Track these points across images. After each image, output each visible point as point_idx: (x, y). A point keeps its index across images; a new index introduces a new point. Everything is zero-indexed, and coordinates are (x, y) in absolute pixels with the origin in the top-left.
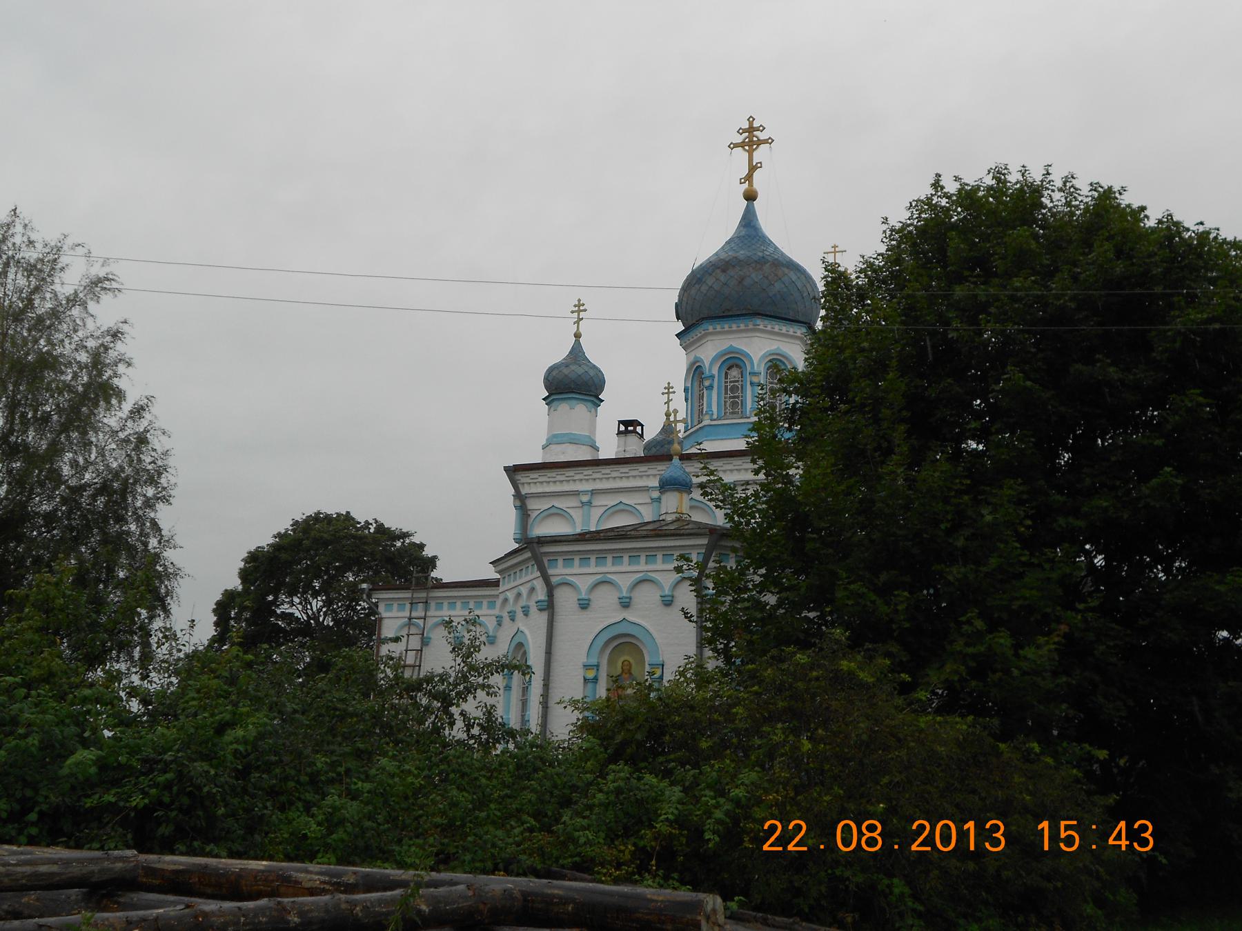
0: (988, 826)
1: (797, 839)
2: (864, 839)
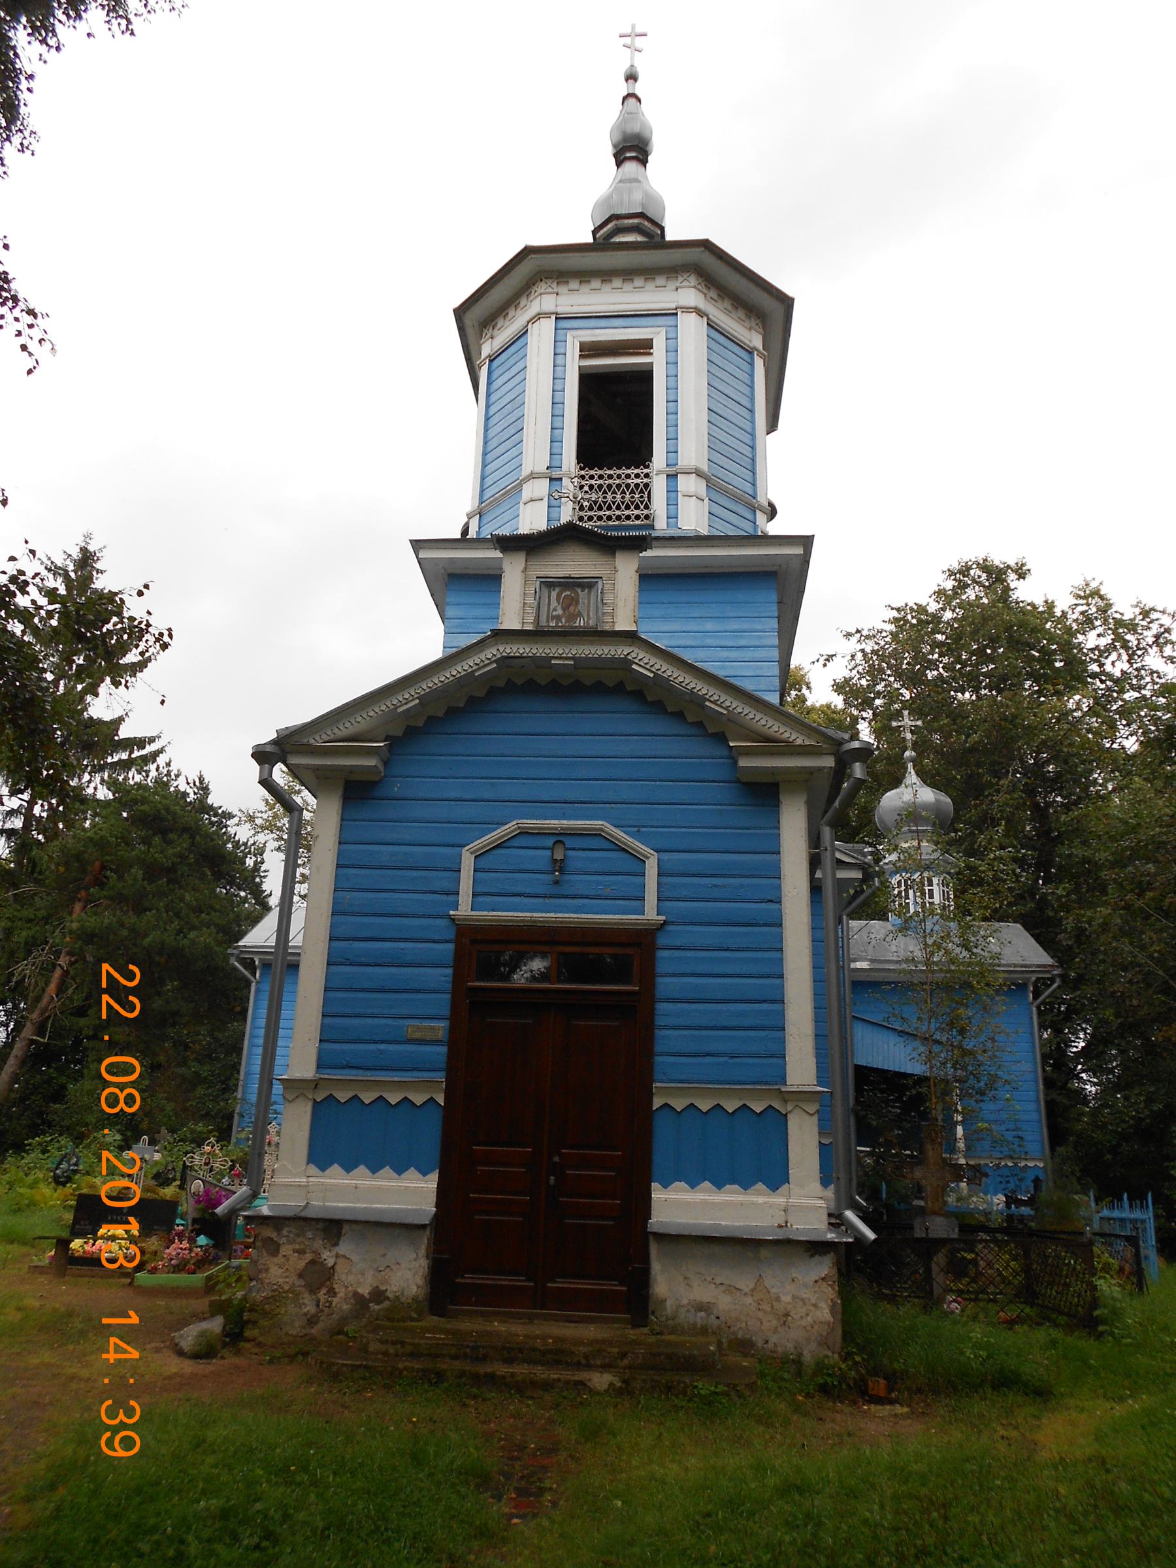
2: (117, 1091)
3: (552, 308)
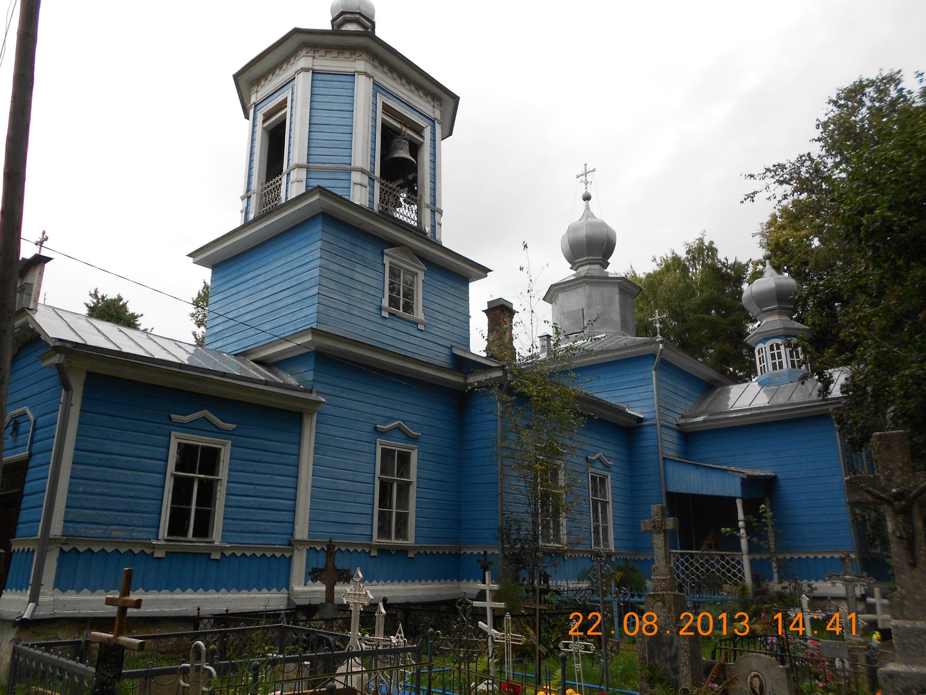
0: (736, 617)
1: (594, 626)
3: (310, 66)
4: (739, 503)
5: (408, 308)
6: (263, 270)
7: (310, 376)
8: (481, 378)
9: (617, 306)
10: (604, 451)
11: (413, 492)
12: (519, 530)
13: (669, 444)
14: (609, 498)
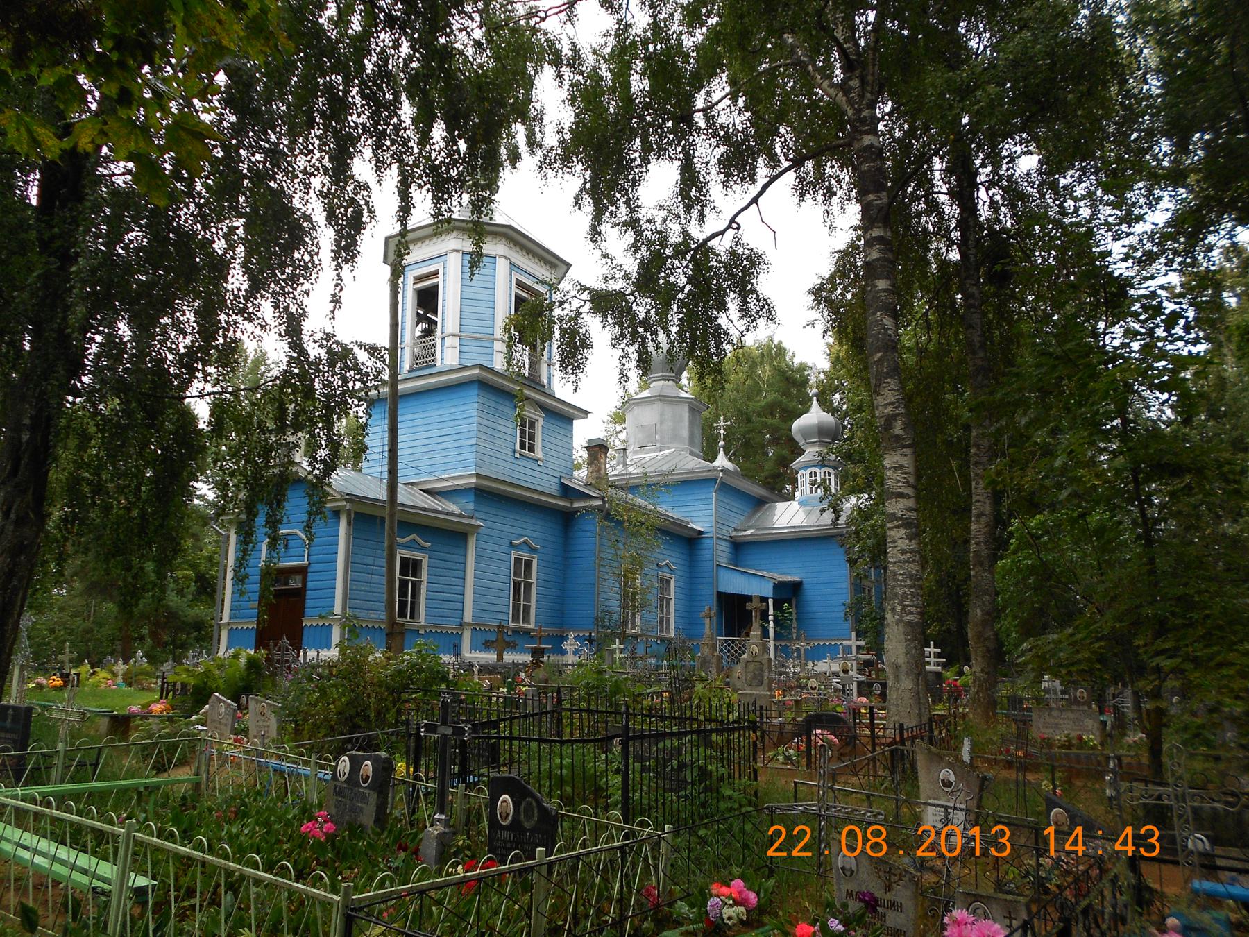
1: (776, 845)
2: (869, 844)
4: (770, 602)
5: (532, 449)
6: (421, 415)
7: (471, 506)
8: (581, 504)
9: (686, 423)
10: (668, 557)
11: (672, 603)
12: (611, 618)
13: (722, 553)
14: (673, 596)
